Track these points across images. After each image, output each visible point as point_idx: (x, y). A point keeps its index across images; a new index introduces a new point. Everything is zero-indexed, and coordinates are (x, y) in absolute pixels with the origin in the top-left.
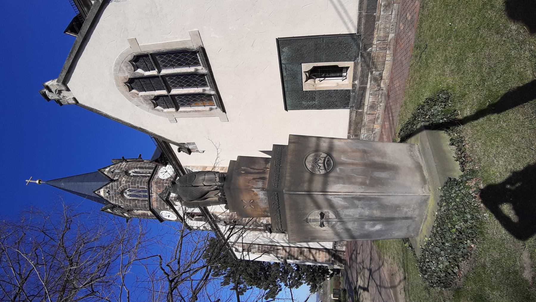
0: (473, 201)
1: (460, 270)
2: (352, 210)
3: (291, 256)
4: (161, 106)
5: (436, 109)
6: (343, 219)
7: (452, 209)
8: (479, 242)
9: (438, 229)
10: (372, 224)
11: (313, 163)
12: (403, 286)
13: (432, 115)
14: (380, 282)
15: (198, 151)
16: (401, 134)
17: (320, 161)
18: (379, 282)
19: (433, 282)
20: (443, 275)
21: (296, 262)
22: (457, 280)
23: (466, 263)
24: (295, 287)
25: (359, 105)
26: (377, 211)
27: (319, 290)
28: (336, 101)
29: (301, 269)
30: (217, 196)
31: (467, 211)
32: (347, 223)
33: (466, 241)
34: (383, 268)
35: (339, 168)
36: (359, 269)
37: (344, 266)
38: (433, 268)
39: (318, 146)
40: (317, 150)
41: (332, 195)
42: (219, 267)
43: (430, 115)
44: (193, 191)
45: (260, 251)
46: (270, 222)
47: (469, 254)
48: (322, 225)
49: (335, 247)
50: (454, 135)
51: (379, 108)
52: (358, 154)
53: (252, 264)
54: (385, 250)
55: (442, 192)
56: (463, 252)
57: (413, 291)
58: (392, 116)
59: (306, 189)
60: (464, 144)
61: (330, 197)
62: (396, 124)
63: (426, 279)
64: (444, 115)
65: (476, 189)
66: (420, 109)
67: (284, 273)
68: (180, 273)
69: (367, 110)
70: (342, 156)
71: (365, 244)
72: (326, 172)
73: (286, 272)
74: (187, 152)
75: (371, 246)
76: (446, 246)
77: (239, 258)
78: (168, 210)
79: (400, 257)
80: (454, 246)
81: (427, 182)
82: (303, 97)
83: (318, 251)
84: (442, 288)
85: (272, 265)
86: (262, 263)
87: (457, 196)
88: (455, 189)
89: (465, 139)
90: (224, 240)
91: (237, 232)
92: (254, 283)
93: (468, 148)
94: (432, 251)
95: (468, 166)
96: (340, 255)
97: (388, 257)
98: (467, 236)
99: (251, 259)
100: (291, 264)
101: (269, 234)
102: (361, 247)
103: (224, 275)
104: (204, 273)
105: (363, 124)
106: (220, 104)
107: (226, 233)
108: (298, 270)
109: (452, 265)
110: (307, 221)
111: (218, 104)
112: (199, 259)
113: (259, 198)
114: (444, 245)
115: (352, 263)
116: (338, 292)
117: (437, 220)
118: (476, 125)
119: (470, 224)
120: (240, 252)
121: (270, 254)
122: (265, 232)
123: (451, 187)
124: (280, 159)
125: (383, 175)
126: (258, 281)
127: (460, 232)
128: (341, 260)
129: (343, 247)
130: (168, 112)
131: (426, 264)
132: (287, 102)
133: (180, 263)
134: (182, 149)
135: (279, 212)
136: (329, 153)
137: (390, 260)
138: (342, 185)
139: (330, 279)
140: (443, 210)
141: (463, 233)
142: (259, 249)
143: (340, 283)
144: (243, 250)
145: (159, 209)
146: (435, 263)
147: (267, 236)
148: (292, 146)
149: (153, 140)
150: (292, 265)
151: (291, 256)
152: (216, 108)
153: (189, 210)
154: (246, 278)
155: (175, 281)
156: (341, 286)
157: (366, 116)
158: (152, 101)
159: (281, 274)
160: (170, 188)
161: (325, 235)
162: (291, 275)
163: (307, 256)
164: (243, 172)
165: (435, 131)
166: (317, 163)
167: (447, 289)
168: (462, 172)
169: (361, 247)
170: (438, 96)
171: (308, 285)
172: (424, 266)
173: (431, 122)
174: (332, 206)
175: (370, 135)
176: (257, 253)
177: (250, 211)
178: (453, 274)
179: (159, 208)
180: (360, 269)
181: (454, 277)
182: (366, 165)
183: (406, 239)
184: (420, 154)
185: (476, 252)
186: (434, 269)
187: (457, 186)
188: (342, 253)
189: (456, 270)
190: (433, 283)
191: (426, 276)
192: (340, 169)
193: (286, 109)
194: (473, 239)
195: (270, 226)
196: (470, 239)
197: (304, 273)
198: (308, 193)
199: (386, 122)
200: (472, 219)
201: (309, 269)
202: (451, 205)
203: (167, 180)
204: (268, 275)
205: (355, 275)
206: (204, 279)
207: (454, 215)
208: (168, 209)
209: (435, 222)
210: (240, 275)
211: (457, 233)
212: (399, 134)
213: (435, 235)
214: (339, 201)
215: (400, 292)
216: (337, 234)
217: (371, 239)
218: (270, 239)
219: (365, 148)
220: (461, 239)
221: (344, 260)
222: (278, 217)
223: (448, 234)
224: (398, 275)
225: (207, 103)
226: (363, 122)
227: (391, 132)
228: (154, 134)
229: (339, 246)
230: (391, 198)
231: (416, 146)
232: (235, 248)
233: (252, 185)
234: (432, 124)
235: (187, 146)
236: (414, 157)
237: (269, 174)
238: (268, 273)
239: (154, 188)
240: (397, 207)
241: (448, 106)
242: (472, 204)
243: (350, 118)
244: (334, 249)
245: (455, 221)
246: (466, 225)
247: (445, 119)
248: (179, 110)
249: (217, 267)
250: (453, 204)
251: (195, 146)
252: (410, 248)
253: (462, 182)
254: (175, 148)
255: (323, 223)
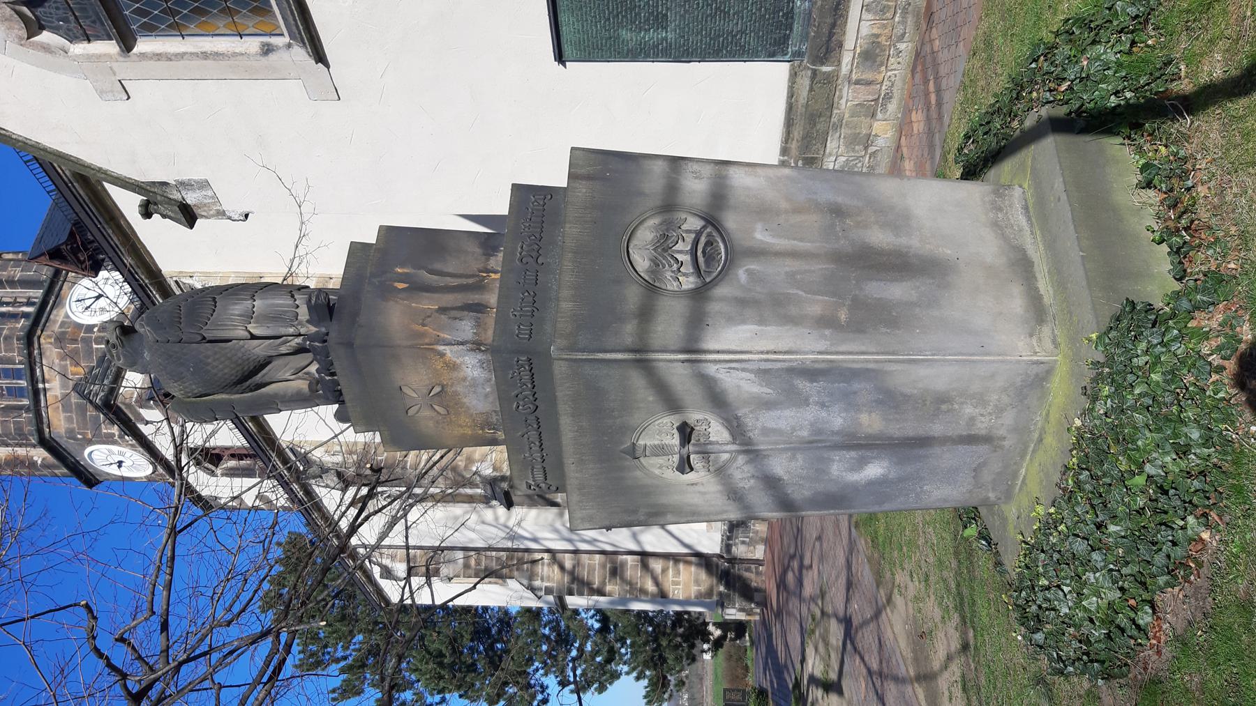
0: (1211, 380)
1: (1158, 618)
2: (787, 413)
3: (579, 584)
4: (55, 30)
5: (1098, 59)
6: (757, 445)
7: (1134, 408)
8: (1228, 524)
9: (1081, 477)
10: (854, 458)
11: (654, 249)
12: (958, 673)
13: (1082, 79)
14: (881, 662)
15: (221, 214)
16: (966, 151)
17: (680, 246)
18: (878, 659)
19: (1064, 658)
20: (1098, 633)
21: (597, 601)
22: (1150, 652)
23: (1181, 596)
24: (596, 689)
25: (824, 49)
26: (873, 415)
27: (675, 694)
28: (742, 32)
29: (616, 626)
30: (306, 373)
31: (1190, 414)
32: (768, 456)
33: (1183, 519)
34: (889, 613)
35: (747, 270)
36: (810, 619)
37: (758, 611)
38: (1065, 610)
39: (672, 188)
40: (669, 205)
41: (720, 361)
42: (322, 635)
43: (1072, 81)
44: (208, 357)
45: (472, 572)
46: (506, 470)
47: (1193, 566)
48: (685, 465)
49: (728, 548)
50: (1156, 151)
51: (892, 60)
52: (813, 221)
53: (442, 617)
54: (896, 552)
55: (1100, 348)
56: (1172, 555)
57: (994, 688)
58: (938, 91)
59: (629, 340)
60: (1190, 183)
61: (711, 370)
62: (951, 119)
63: (1041, 647)
64: (1125, 78)
65: (1223, 340)
66: (1039, 57)
67: (556, 642)
68: (172, 665)
69: (849, 67)
70: (759, 226)
71: (829, 532)
72: (700, 284)
73: (563, 640)
74: (180, 216)
75: (850, 538)
76: (1110, 535)
77: (395, 598)
78: (114, 443)
79: (949, 575)
80: (1137, 537)
81: (1050, 318)
82: (621, 12)
83: (671, 563)
84: (1096, 677)
85: (515, 618)
86: (480, 611)
87: (1155, 364)
88: (1146, 338)
89: (1198, 167)
90: (338, 537)
91: (384, 507)
92: (451, 684)
93: (1206, 197)
94: (1059, 552)
95: (1202, 262)
96: (747, 575)
97: (908, 578)
98: (1185, 502)
99: (438, 602)
100: (581, 610)
101: (501, 510)
102: (817, 544)
103: (342, 664)
104: (264, 659)
105: (836, 120)
106: (301, 27)
107: (345, 512)
108: (604, 629)
109: (1132, 602)
110: (633, 452)
111: (294, 28)
112: (243, 610)
113: (464, 379)
114: (1104, 530)
115: (787, 599)
116: (739, 701)
117: (1077, 446)
118: (1241, 113)
119: (1198, 462)
120: (396, 579)
121: (509, 581)
122: (491, 507)
123: (1133, 333)
124: (538, 236)
125: (897, 291)
126: (465, 676)
127: (1161, 485)
128: (747, 592)
129: (757, 546)
130: (89, 58)
131: (1040, 595)
132: (564, 30)
133: (171, 629)
134: (156, 204)
135: (535, 426)
136: (712, 217)
137: (914, 587)
138: (755, 326)
139: (712, 657)
140: (1102, 412)
141: (1172, 492)
142: (466, 566)
143: (746, 669)
144: (410, 572)
145: (77, 439)
146: (1070, 592)
147: (497, 519)
148: (583, 189)
149: (34, 172)
150: (583, 615)
151: (579, 584)
152: (289, 46)
153: (198, 435)
154: (423, 667)
155: (154, 694)
156: (751, 680)
157: (846, 88)
158: (17, 7)
159: (545, 648)
160: (114, 351)
161: (693, 499)
162: (581, 650)
163: (634, 581)
164: (401, 286)
165: (1087, 138)
166: (669, 251)
167: (1115, 683)
168: (1177, 280)
169: (817, 544)
170: (1109, 9)
171: (638, 679)
172: (1030, 604)
173: (1075, 105)
174: (717, 400)
175: (858, 158)
176: (462, 579)
177: (431, 424)
178: (1135, 633)
179: (79, 436)
180: (814, 619)
181: (1140, 641)
182: (838, 258)
183: (967, 511)
184: (1029, 219)
185: (1217, 558)
186: (1066, 614)
187: (1154, 330)
188: (753, 566)
189: (1145, 618)
190: (1063, 662)
191: (1039, 637)
192: (750, 273)
193: (560, 58)
194: (1207, 511)
195: (505, 485)
196: (1199, 511)
197: (626, 639)
198: (638, 356)
199: (914, 112)
200: (1207, 442)
201: (643, 625)
202: (1131, 393)
203: (103, 327)
204: (499, 652)
205: (794, 639)
206: (265, 679)
207: (1142, 430)
208: (116, 438)
209: (1071, 451)
210: (400, 658)
211: (1151, 491)
212: (960, 150)
213: (1070, 498)
214: (742, 383)
215: (950, 693)
216: (735, 495)
217: (848, 511)
218: (507, 527)
219: (840, 199)
220: (1166, 512)
221: (757, 590)
222: (532, 443)
223: (1116, 494)
224: (941, 635)
225: (250, 23)
226: (835, 111)
227: (931, 147)
228: (37, 147)
229: (743, 542)
230: (923, 371)
231: (1017, 192)
232: (380, 565)
233: (438, 334)
234: (1079, 112)
235: (176, 196)
236: (1008, 231)
237: (497, 291)
238: (499, 646)
239: (51, 355)
240: (941, 402)
241: (1142, 45)
242: (1208, 393)
243: (791, 94)
244: (725, 555)
245: (1144, 451)
246: (1183, 464)
247: (1128, 95)
248: (135, 50)
249: (315, 637)
250: (1137, 391)
251: (210, 193)
252: (984, 543)
253: (1173, 315)
254: (128, 203)
255: (688, 457)
